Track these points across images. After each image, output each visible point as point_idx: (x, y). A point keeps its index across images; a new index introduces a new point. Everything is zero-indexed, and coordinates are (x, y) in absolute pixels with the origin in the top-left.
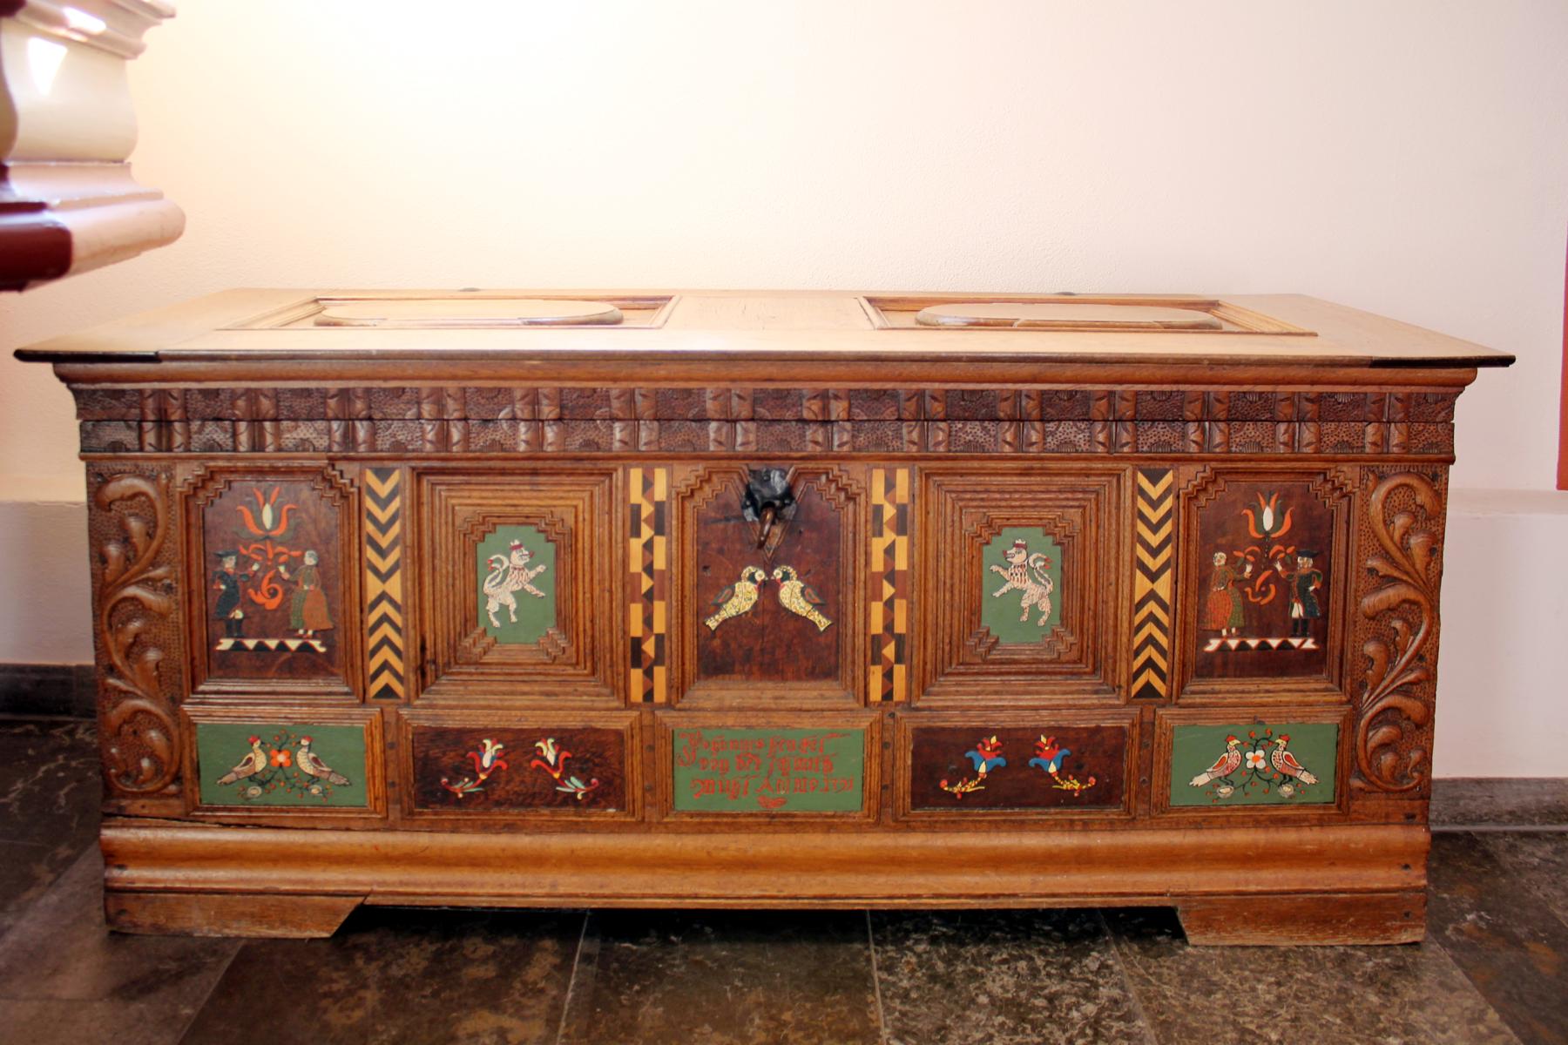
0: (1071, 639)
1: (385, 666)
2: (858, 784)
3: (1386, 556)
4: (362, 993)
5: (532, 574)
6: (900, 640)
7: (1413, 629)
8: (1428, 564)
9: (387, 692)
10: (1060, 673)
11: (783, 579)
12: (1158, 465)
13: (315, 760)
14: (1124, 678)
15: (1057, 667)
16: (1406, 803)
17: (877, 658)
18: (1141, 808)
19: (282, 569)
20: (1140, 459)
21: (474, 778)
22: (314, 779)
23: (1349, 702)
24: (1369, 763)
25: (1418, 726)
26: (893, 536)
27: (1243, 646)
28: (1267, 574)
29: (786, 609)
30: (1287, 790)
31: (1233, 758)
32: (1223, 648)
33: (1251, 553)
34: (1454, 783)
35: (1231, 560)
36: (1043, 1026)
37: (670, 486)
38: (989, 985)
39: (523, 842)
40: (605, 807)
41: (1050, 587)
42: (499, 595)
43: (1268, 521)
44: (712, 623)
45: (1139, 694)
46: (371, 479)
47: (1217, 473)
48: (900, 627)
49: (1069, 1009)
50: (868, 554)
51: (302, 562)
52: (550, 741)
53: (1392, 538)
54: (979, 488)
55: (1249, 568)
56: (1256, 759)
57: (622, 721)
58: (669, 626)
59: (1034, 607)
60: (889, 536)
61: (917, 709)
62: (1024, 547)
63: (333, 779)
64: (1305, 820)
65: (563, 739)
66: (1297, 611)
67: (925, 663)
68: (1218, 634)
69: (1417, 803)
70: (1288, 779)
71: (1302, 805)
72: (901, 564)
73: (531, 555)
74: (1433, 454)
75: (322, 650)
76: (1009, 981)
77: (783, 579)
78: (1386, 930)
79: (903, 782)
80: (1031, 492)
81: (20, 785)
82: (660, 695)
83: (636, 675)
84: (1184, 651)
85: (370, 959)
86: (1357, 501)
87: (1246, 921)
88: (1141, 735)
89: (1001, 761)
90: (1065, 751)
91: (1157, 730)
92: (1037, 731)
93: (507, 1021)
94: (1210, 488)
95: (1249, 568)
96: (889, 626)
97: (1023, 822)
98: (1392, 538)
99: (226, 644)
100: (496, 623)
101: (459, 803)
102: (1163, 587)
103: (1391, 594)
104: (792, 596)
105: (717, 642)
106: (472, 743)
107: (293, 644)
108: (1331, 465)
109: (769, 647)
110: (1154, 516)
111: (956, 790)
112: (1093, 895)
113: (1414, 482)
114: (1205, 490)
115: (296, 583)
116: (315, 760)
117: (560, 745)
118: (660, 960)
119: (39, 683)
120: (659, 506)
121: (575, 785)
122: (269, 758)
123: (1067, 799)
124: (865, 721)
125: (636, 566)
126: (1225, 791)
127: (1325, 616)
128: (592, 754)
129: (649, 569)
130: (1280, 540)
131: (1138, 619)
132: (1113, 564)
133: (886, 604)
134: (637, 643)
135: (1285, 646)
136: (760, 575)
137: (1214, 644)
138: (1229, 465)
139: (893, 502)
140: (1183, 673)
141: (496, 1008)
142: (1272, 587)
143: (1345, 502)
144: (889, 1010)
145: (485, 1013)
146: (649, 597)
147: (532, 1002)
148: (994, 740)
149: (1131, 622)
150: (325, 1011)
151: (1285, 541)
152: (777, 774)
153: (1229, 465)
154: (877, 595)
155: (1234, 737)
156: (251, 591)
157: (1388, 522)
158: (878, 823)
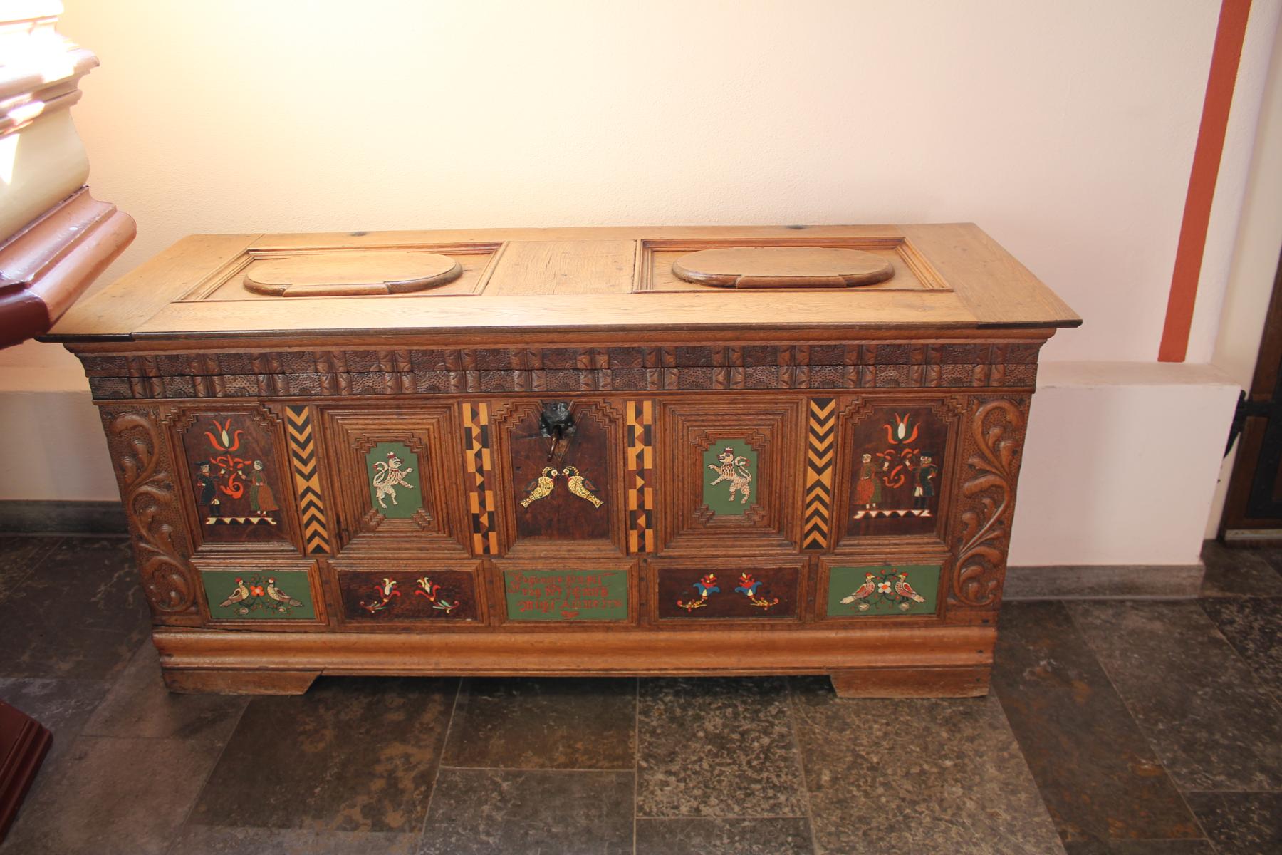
0: (763, 513)
3: (983, 457)
5: (404, 474)
6: (649, 514)
7: (996, 504)
9: (318, 549)
13: (279, 592)
14: (798, 537)
17: (634, 526)
18: (809, 616)
21: (380, 601)
22: (280, 603)
27: (880, 515)
28: (899, 468)
30: (905, 606)
31: (869, 586)
32: (867, 516)
37: (490, 415)
41: (749, 478)
42: (384, 488)
43: (901, 432)
44: (525, 504)
45: (809, 547)
47: (866, 401)
48: (649, 505)
55: (886, 464)
56: (885, 587)
57: (471, 566)
58: (496, 507)
59: (738, 492)
60: (639, 446)
63: (292, 602)
65: (434, 577)
66: (919, 492)
68: (863, 508)
70: (905, 599)
78: (964, 689)
81: (103, 588)
82: (494, 550)
83: (478, 537)
84: (839, 519)
89: (717, 589)
92: (740, 571)
93: (410, 749)
95: (886, 464)
96: (641, 504)
99: (212, 521)
102: (826, 478)
104: (576, 485)
105: (528, 516)
107: (255, 520)
109: (562, 518)
113: (1004, 404)
116: (279, 592)
120: (484, 428)
121: (444, 605)
122: (250, 591)
123: (760, 612)
124: (627, 565)
125: (471, 468)
126: (863, 606)
127: (938, 495)
128: (449, 584)
129: (480, 470)
130: (909, 445)
131: (808, 499)
134: (476, 517)
135: (909, 515)
137: (861, 514)
139: (641, 424)
141: (404, 741)
146: (482, 488)
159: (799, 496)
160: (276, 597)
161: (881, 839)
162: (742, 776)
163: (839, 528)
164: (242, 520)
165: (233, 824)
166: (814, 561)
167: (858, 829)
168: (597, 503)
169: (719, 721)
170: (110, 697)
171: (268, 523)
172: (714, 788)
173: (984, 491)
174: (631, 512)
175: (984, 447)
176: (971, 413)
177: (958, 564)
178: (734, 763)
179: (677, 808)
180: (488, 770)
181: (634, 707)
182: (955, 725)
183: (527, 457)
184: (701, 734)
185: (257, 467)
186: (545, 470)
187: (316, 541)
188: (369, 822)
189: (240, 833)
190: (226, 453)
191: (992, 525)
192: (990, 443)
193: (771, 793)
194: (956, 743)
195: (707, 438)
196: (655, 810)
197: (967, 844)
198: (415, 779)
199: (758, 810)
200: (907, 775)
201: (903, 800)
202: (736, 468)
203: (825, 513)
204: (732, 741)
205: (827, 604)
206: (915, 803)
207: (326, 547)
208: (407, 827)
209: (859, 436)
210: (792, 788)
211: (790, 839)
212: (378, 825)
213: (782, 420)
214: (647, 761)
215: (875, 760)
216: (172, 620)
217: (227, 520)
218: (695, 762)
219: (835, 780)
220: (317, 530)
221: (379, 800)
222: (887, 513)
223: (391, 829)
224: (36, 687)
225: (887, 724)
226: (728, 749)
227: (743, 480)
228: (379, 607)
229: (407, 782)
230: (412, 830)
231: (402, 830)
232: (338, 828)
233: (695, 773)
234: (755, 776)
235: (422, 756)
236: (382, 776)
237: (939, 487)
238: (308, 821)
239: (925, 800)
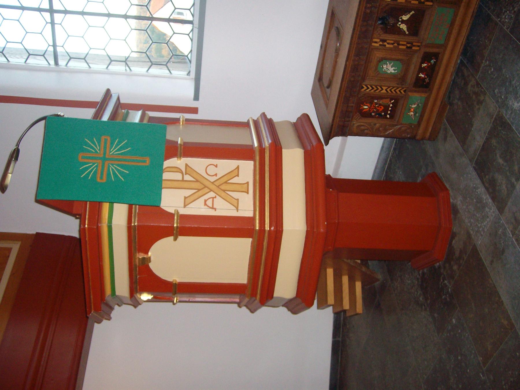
9: (405, 91)
21: (426, 78)
22: (418, 105)
39: (441, 72)
44: (407, 33)
82: (419, 44)
83: (413, 48)
99: (388, 116)
104: (405, 18)
107: (391, 105)
120: (380, 41)
121: (432, 61)
125: (392, 46)
128: (426, 57)
129: (392, 44)
134: (408, 47)
146: (399, 44)
160: (416, 106)
168: (413, 12)
174: (419, 3)
179: (511, 18)
180: (483, 65)
185: (376, 101)
186: (398, 25)
187: (402, 91)
189: (469, 138)
190: (370, 108)
207: (404, 89)
220: (400, 92)
224: (423, 171)
229: (476, 90)
231: (485, 97)
235: (473, 82)
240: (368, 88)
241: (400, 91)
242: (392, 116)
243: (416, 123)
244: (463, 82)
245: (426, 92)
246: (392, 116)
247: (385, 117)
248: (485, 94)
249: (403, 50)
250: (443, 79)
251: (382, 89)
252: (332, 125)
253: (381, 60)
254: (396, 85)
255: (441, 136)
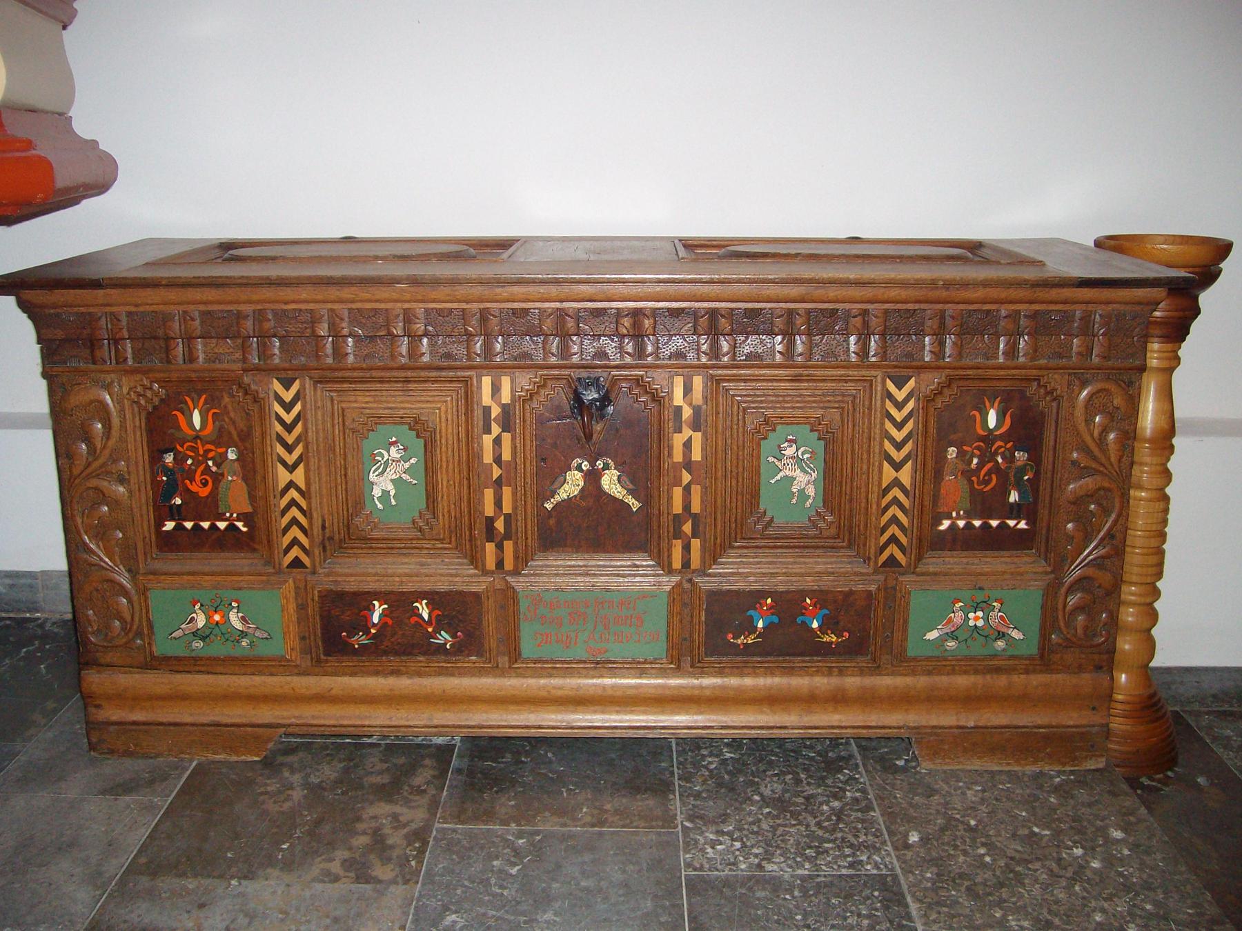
0: (830, 518)
1: (295, 542)
2: (663, 637)
3: (1087, 451)
4: (290, 792)
5: (407, 465)
6: (696, 518)
7: (1106, 512)
8: (1121, 457)
9: (296, 563)
10: (823, 547)
11: (603, 469)
12: (904, 372)
13: (243, 618)
14: (872, 551)
15: (821, 542)
16: (1096, 657)
17: (678, 534)
18: (885, 658)
19: (210, 463)
20: (888, 367)
21: (367, 632)
22: (243, 634)
23: (1052, 572)
24: (1067, 625)
25: (1108, 594)
26: (691, 433)
27: (969, 526)
28: (989, 465)
29: (606, 493)
30: (1001, 644)
31: (958, 618)
32: (953, 527)
33: (978, 448)
34: (1168, 670)
35: (961, 454)
36: (800, 814)
37: (513, 391)
38: (762, 789)
39: (404, 684)
40: (469, 655)
41: (814, 475)
42: (382, 484)
43: (992, 420)
44: (549, 506)
45: (885, 564)
46: (277, 386)
47: (950, 381)
48: (696, 508)
49: (821, 804)
50: (671, 448)
51: (227, 458)
52: (424, 602)
53: (1092, 435)
54: (758, 392)
55: (975, 461)
56: (976, 619)
57: (479, 585)
58: (515, 508)
59: (802, 492)
60: (687, 432)
61: (709, 575)
62: (794, 441)
63: (258, 633)
64: (1015, 669)
65: (434, 599)
66: (1014, 497)
67: (716, 538)
68: (949, 517)
69: (1105, 657)
70: (1002, 635)
71: (1013, 657)
72: (697, 455)
73: (405, 449)
74: (1130, 362)
75: (245, 529)
76: (778, 787)
77: (603, 469)
78: (1075, 759)
79: (699, 636)
80: (800, 396)
81: (7, 661)
82: (509, 564)
83: (490, 547)
84: (920, 528)
85: (293, 771)
86: (1065, 404)
87: (965, 750)
88: (886, 598)
89: (775, 619)
90: (825, 611)
91: (899, 595)
92: (803, 594)
93: (397, 809)
94: (946, 390)
95: (975, 461)
96: (687, 506)
97: (793, 668)
98: (1092, 435)
99: (170, 526)
100: (380, 506)
101: (355, 652)
102: (905, 475)
103: (1089, 483)
104: (611, 482)
105: (552, 522)
106: (364, 604)
107: (222, 525)
108: (1045, 372)
109: (595, 527)
110: (899, 416)
111: (739, 642)
112: (846, 728)
113: (1113, 387)
114: (940, 393)
115: (222, 475)
116: (243, 618)
117: (432, 605)
118: (513, 773)
119: (12, 586)
120: (505, 407)
121: (444, 637)
122: (209, 618)
123: (824, 650)
124: (668, 582)
125: (488, 458)
126: (951, 644)
127: (1036, 502)
128: (455, 609)
129: (498, 460)
130: (1001, 437)
131: (884, 503)
132: (865, 456)
133: (684, 489)
134: (490, 521)
135: (1003, 526)
136: (586, 466)
137: (946, 524)
138: (962, 372)
139: (690, 404)
140: (920, 547)
141: (391, 801)
142: (994, 477)
143: (1054, 404)
144: (683, 803)
145: (383, 804)
146: (499, 483)
147: (417, 798)
148: (769, 601)
149: (878, 504)
150: (263, 802)
151: (1005, 437)
152: (600, 628)
153: (962, 372)
154: (678, 482)
155: (958, 601)
156: (187, 482)
157: (1089, 421)
158: (679, 667)
159: (873, 498)
160: (239, 626)
161: (990, 894)
162: (812, 836)
163: (920, 540)
164: (206, 525)
165: (183, 875)
166: (891, 583)
167: (960, 885)
169: (778, 787)
170: (22, 758)
171: (237, 528)
172: (777, 847)
173: (1090, 496)
175: (1088, 439)
176: (1073, 399)
177: (1063, 590)
178: (800, 824)
181: (672, 773)
182: (1067, 792)
183: (554, 445)
184: (757, 798)
185: (232, 455)
187: (295, 552)
188: (352, 875)
189: (191, 884)
191: (1102, 539)
192: (1096, 433)
193: (847, 851)
194: (1069, 808)
195: (767, 421)
196: (707, 866)
197: (1096, 899)
198: (406, 837)
199: (834, 866)
200: (1014, 835)
201: (1012, 858)
202: (798, 461)
203: (904, 520)
204: (797, 804)
205: (906, 639)
206: (1028, 862)
207: (305, 559)
208: (399, 879)
209: (943, 424)
210: (874, 847)
211: (876, 893)
212: (363, 877)
213: (853, 402)
214: (692, 822)
215: (973, 823)
216: (109, 658)
217: (189, 525)
218: (753, 823)
219: (924, 840)
220: (291, 539)
221: (363, 855)
222: (977, 523)
223: (380, 882)
225: (984, 791)
226: (791, 812)
227: (807, 478)
228: (364, 640)
229: (395, 838)
230: (406, 882)
231: (394, 882)
232: (313, 880)
233: (753, 833)
234: (827, 835)
235: (415, 815)
236: (364, 833)
237: (1038, 491)
238: (275, 872)
239: (1038, 859)
240: (288, 407)
241: (295, 542)
242: (168, 543)
243: (162, 647)
244: (385, 779)
245: (306, 651)
246: (168, 543)
247: (164, 510)
248: (408, 878)
249: (474, 505)
250: (371, 700)
251: (291, 468)
252: (96, 284)
253: (418, 426)
254: (317, 523)
255: (115, 768)
